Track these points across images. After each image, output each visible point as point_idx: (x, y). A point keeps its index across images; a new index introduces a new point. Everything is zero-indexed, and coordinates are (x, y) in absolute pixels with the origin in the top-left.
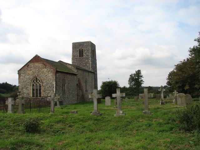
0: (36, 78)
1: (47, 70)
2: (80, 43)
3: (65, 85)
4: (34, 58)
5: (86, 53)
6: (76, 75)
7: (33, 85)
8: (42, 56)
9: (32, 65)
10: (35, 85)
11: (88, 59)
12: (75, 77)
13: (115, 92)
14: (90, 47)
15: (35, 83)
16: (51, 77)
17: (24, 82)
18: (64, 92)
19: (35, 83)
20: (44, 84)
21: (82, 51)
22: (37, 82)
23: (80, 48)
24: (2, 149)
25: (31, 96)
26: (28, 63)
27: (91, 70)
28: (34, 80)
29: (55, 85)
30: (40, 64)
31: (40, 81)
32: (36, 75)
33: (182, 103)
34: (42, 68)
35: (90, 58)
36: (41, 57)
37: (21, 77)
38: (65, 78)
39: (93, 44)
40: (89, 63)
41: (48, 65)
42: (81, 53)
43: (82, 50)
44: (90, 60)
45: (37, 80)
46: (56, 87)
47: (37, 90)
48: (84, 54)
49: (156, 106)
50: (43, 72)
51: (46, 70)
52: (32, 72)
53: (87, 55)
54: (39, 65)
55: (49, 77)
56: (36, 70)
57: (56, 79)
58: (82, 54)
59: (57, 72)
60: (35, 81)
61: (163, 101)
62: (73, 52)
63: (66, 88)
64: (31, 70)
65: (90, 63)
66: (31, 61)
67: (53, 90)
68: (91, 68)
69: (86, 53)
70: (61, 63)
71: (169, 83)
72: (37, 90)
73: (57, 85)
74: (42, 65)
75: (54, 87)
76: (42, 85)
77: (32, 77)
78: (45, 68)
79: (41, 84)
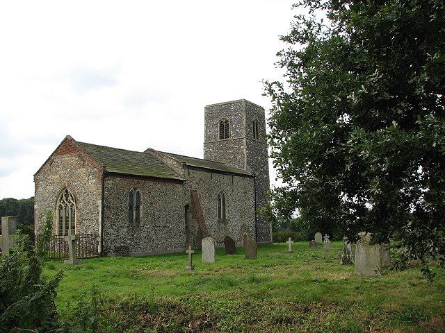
0: (67, 191)
3: (138, 207)
4: (62, 143)
5: (234, 130)
6: (181, 182)
7: (61, 208)
8: (79, 138)
9: (58, 160)
10: (64, 207)
11: (239, 142)
12: (180, 187)
14: (244, 114)
15: (63, 203)
16: (93, 188)
18: (134, 222)
19: (63, 203)
20: (80, 205)
21: (227, 125)
22: (67, 200)
24: (328, 319)
25: (57, 233)
27: (246, 169)
29: (100, 208)
31: (72, 199)
33: (368, 265)
35: (244, 141)
36: (77, 140)
37: (40, 189)
38: (139, 190)
39: (254, 105)
40: (242, 153)
41: (87, 158)
42: (224, 130)
43: (227, 121)
44: (245, 144)
46: (102, 213)
47: (67, 218)
48: (231, 132)
50: (78, 176)
51: (84, 170)
53: (237, 134)
54: (71, 159)
55: (89, 185)
57: (103, 192)
58: (227, 131)
59: (106, 175)
60: (64, 198)
61: (349, 253)
62: (207, 127)
63: (141, 216)
65: (245, 152)
66: (58, 152)
67: (97, 220)
68: (248, 164)
69: (234, 130)
70: (151, 153)
72: (67, 218)
73: (109, 208)
75: (98, 213)
76: (77, 208)
77: (58, 189)
79: (74, 203)
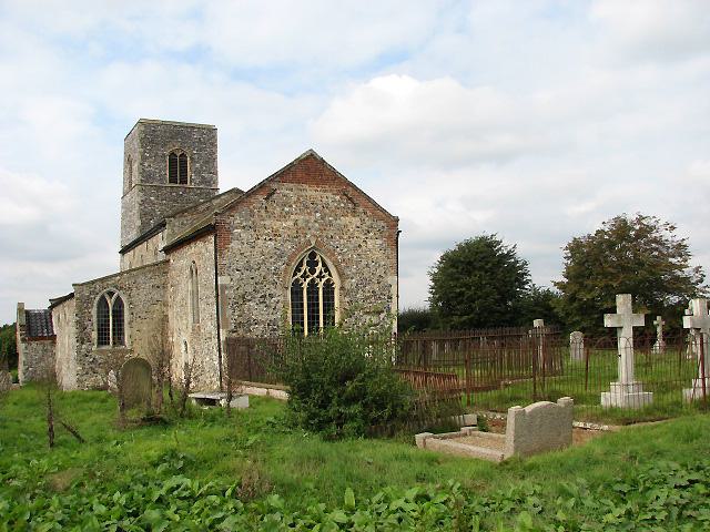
1: (363, 221)
2: (183, 126)
9: (285, 190)
13: (613, 310)
17: (249, 269)
23: (175, 146)
25: (434, 347)
26: (271, 179)
28: (301, 264)
30: (329, 194)
32: (313, 243)
34: (338, 212)
45: (312, 264)
49: (164, 439)
50: (342, 230)
51: (356, 221)
52: (290, 223)
56: (313, 219)
58: (184, 171)
64: (285, 216)
66: (284, 175)
69: (198, 172)
71: (434, 301)
74: (338, 198)
78: (354, 213)
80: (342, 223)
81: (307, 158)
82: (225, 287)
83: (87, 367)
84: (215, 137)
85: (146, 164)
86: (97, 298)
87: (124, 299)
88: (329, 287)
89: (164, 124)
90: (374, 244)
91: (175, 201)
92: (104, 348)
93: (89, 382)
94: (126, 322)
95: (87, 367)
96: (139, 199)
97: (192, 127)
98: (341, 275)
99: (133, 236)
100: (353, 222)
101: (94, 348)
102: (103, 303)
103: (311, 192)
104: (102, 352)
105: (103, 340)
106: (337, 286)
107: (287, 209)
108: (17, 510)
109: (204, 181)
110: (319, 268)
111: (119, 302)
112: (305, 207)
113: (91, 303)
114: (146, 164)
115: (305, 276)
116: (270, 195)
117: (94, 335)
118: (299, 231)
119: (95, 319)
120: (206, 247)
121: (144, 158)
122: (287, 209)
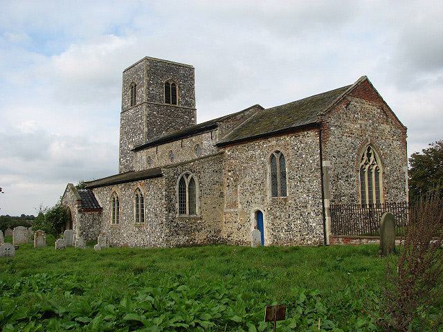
2: (173, 64)
28: (363, 155)
32: (369, 140)
34: (380, 120)
52: (359, 126)
64: (355, 121)
69: (183, 97)
74: (379, 110)
80: (382, 128)
81: (364, 82)
82: (328, 168)
83: (173, 230)
84: (193, 74)
85: (151, 89)
86: (180, 178)
87: (196, 179)
88: (377, 170)
89: (161, 61)
90: (396, 144)
91: (169, 116)
92: (183, 216)
93: (174, 241)
94: (197, 196)
95: (173, 230)
96: (146, 113)
97: (179, 66)
98: (383, 163)
99: (142, 139)
100: (386, 128)
101: (177, 215)
102: (182, 181)
103: (368, 106)
104: (182, 219)
105: (182, 211)
106: (381, 172)
107: (356, 116)
108: (405, 323)
109: (187, 103)
110: (372, 157)
111: (192, 180)
112: (366, 115)
113: (175, 181)
114: (151, 89)
115: (366, 164)
116: (348, 105)
117: (177, 205)
118: (363, 131)
119: (177, 193)
120: (311, 137)
121: (149, 85)
122: (356, 116)
